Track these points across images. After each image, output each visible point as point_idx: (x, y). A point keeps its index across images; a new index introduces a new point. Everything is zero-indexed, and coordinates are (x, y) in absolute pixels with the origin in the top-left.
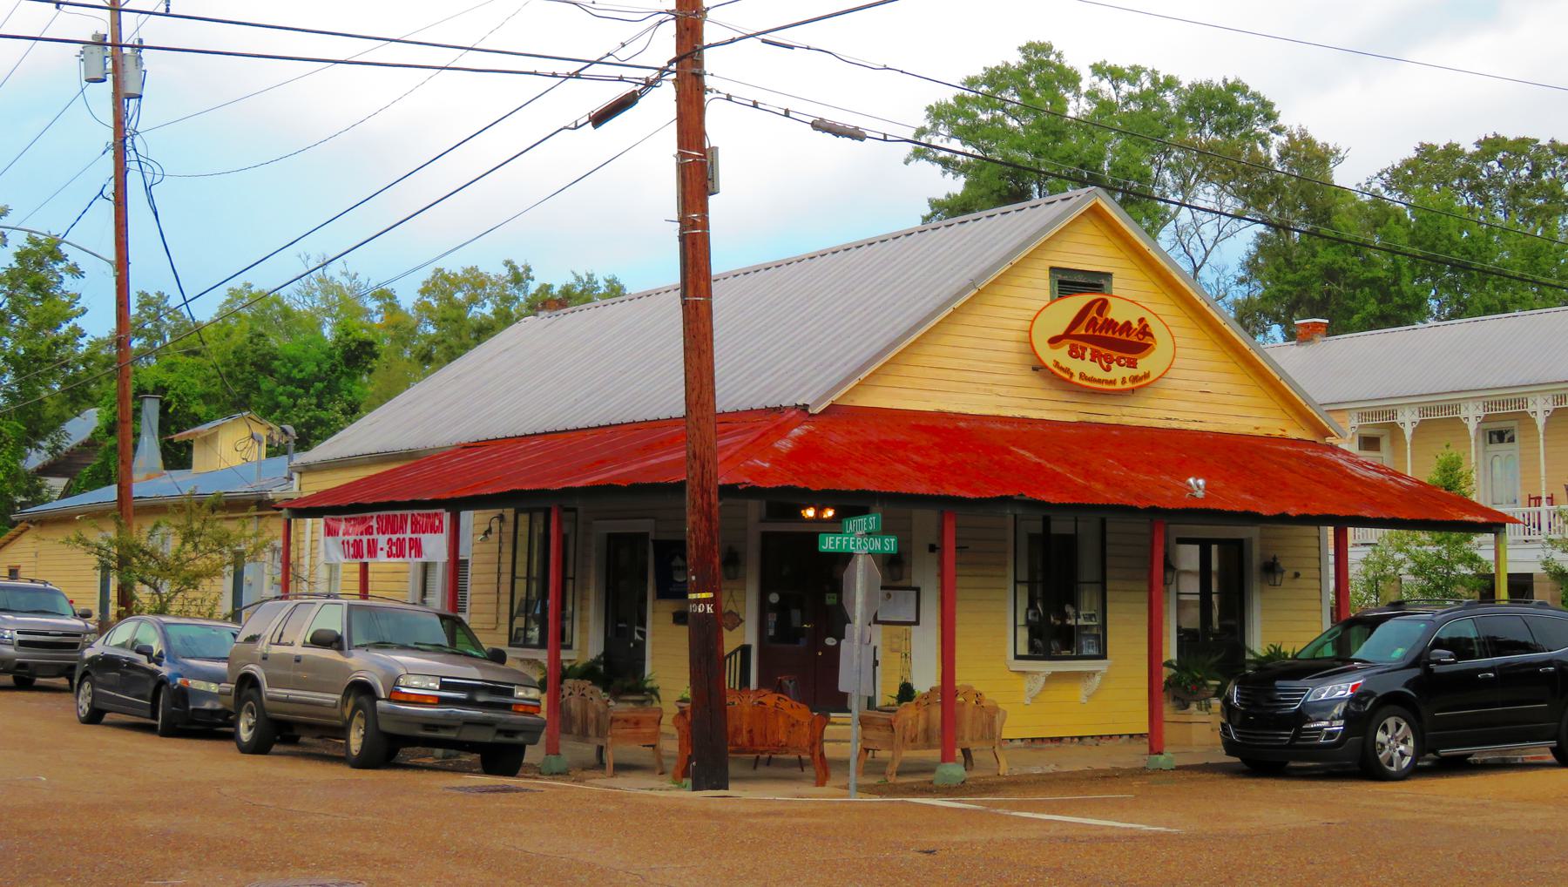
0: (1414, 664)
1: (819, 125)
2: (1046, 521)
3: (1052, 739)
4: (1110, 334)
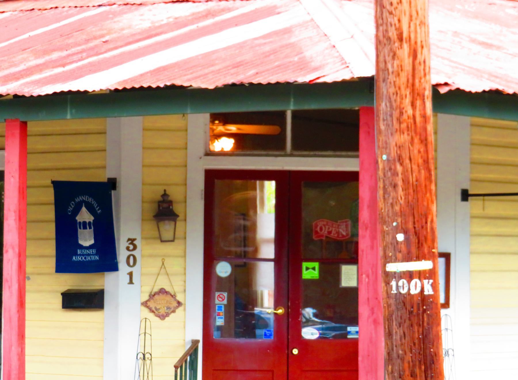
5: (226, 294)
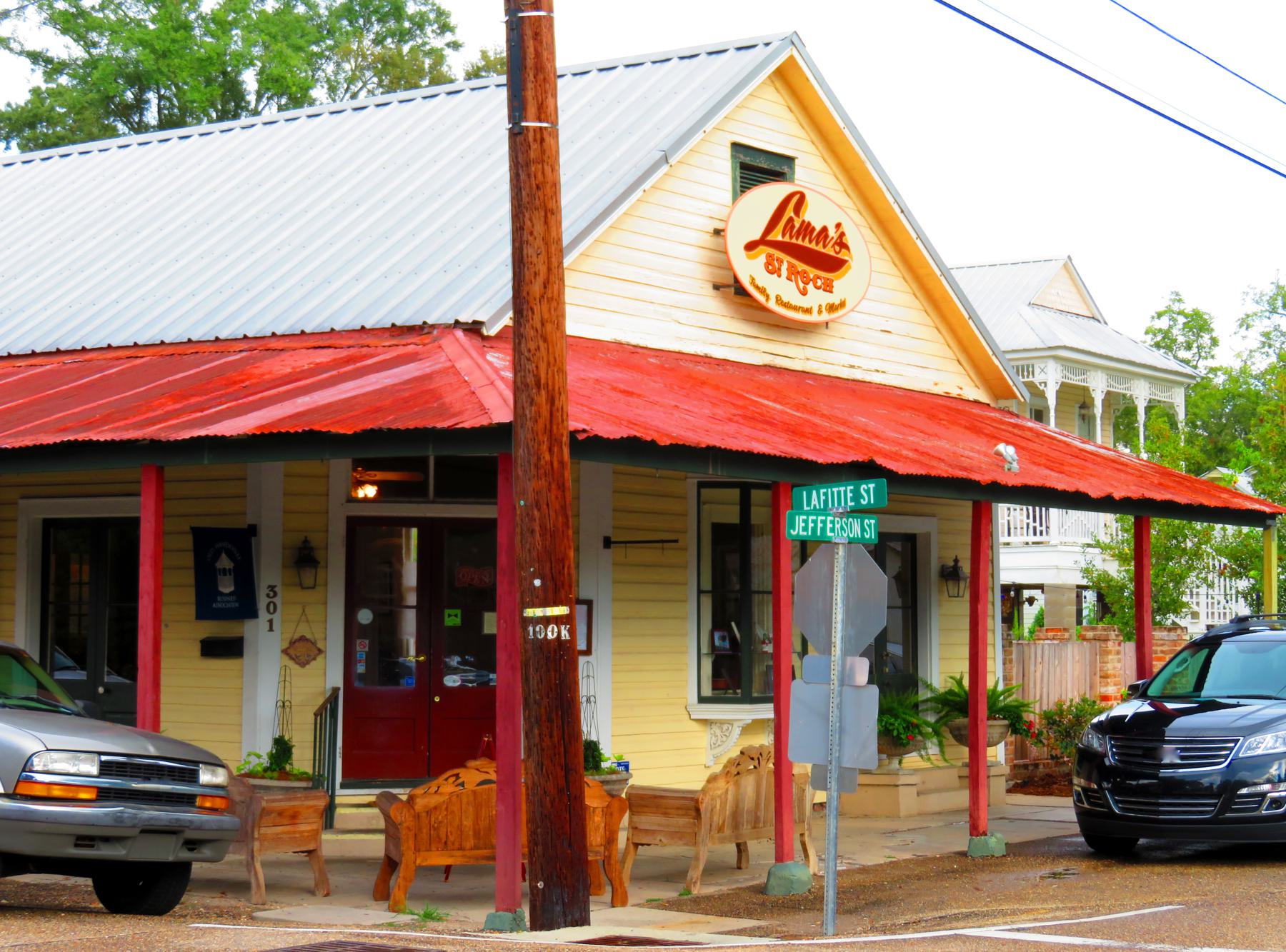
5: (367, 642)
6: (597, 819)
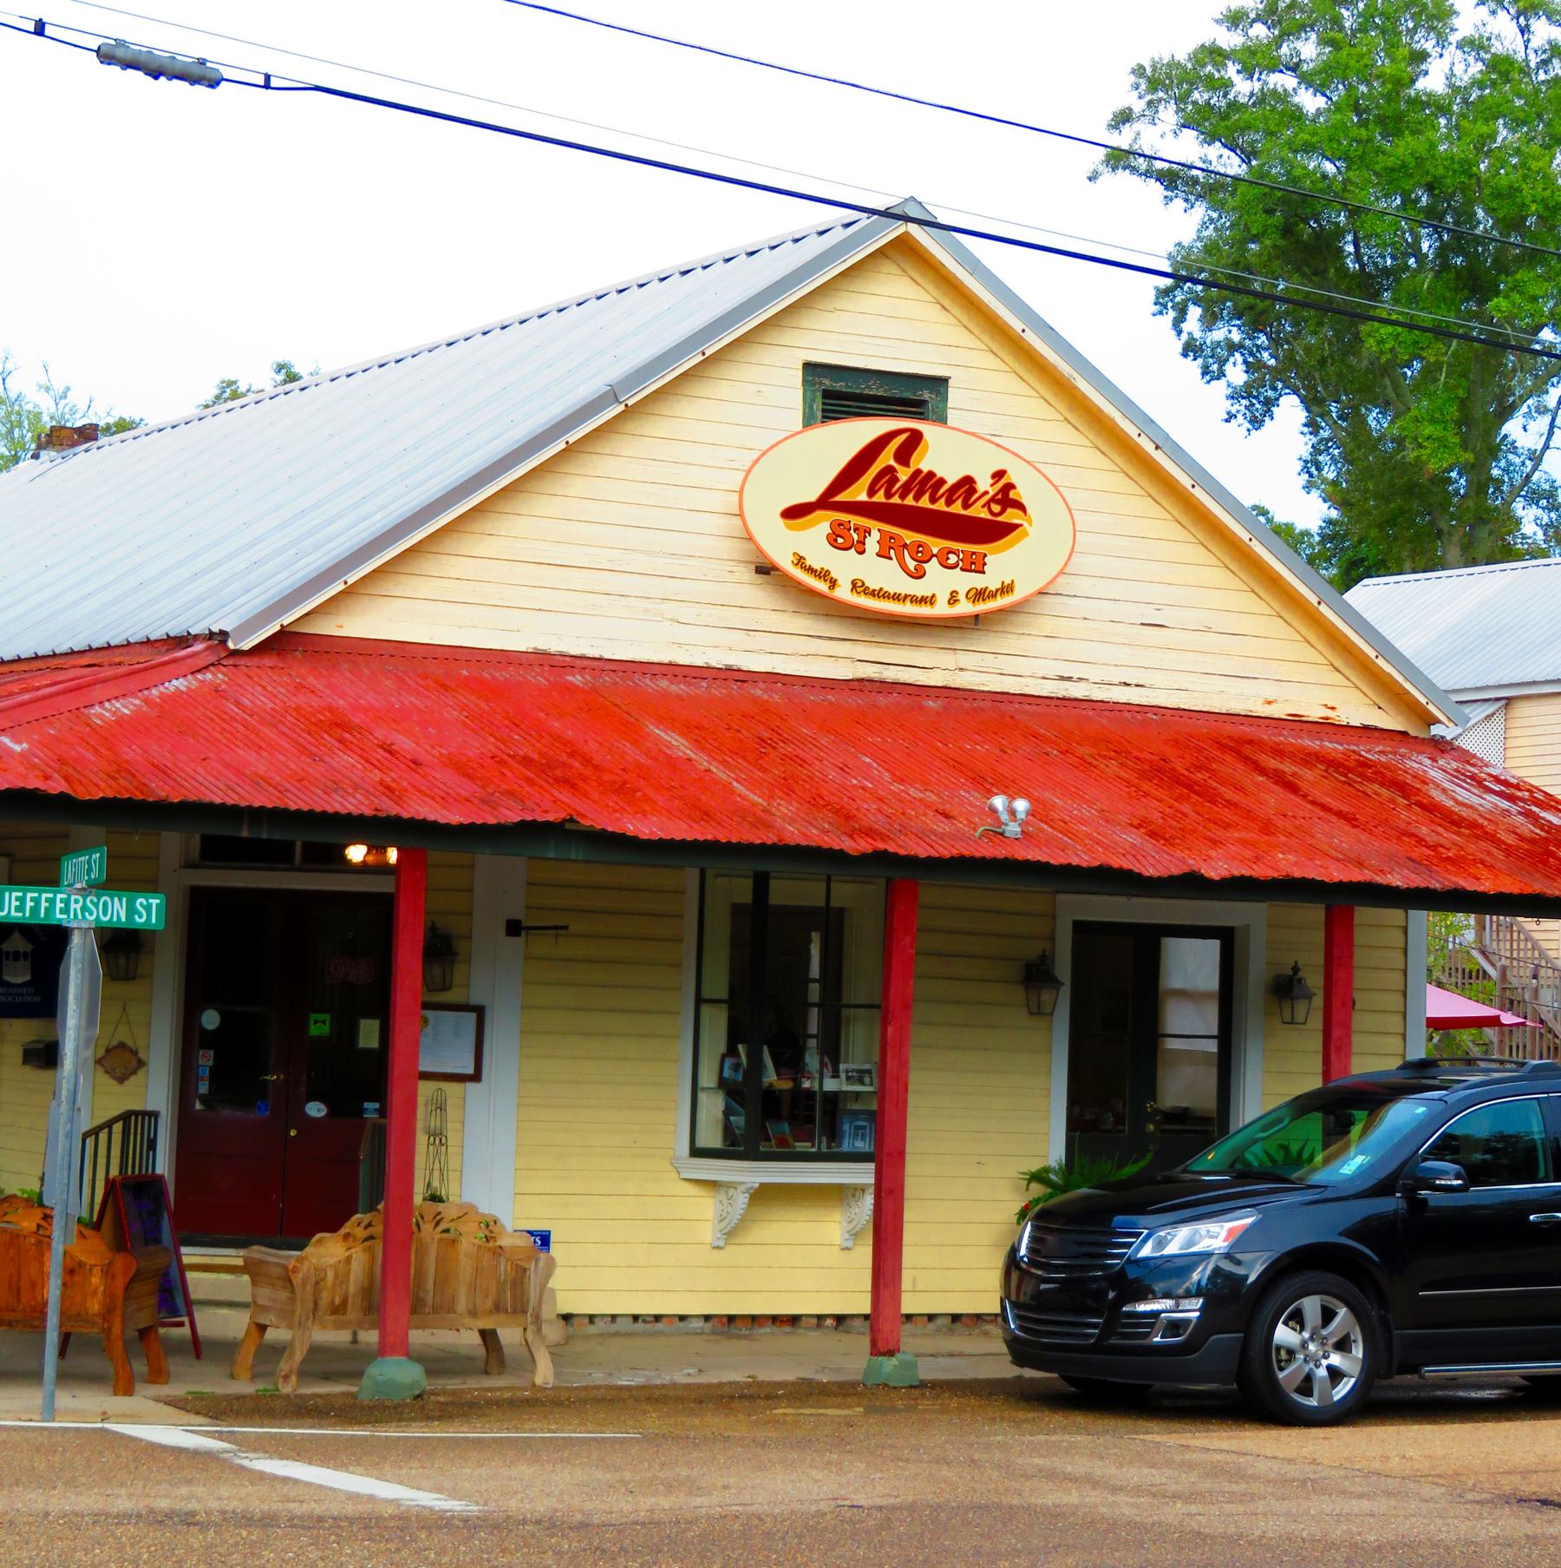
0: (1383, 1188)
1: (113, 55)
2: (761, 883)
3: (775, 1319)
4: (925, 502)
5: (212, 1053)
6: (95, 1280)
